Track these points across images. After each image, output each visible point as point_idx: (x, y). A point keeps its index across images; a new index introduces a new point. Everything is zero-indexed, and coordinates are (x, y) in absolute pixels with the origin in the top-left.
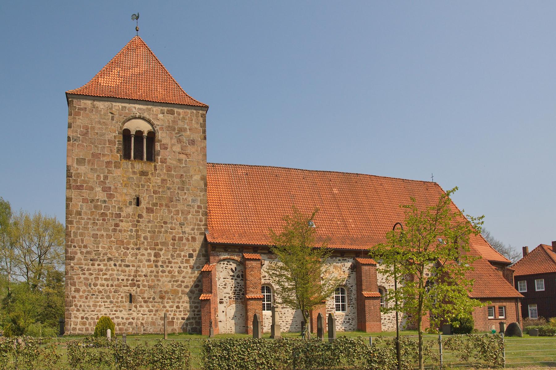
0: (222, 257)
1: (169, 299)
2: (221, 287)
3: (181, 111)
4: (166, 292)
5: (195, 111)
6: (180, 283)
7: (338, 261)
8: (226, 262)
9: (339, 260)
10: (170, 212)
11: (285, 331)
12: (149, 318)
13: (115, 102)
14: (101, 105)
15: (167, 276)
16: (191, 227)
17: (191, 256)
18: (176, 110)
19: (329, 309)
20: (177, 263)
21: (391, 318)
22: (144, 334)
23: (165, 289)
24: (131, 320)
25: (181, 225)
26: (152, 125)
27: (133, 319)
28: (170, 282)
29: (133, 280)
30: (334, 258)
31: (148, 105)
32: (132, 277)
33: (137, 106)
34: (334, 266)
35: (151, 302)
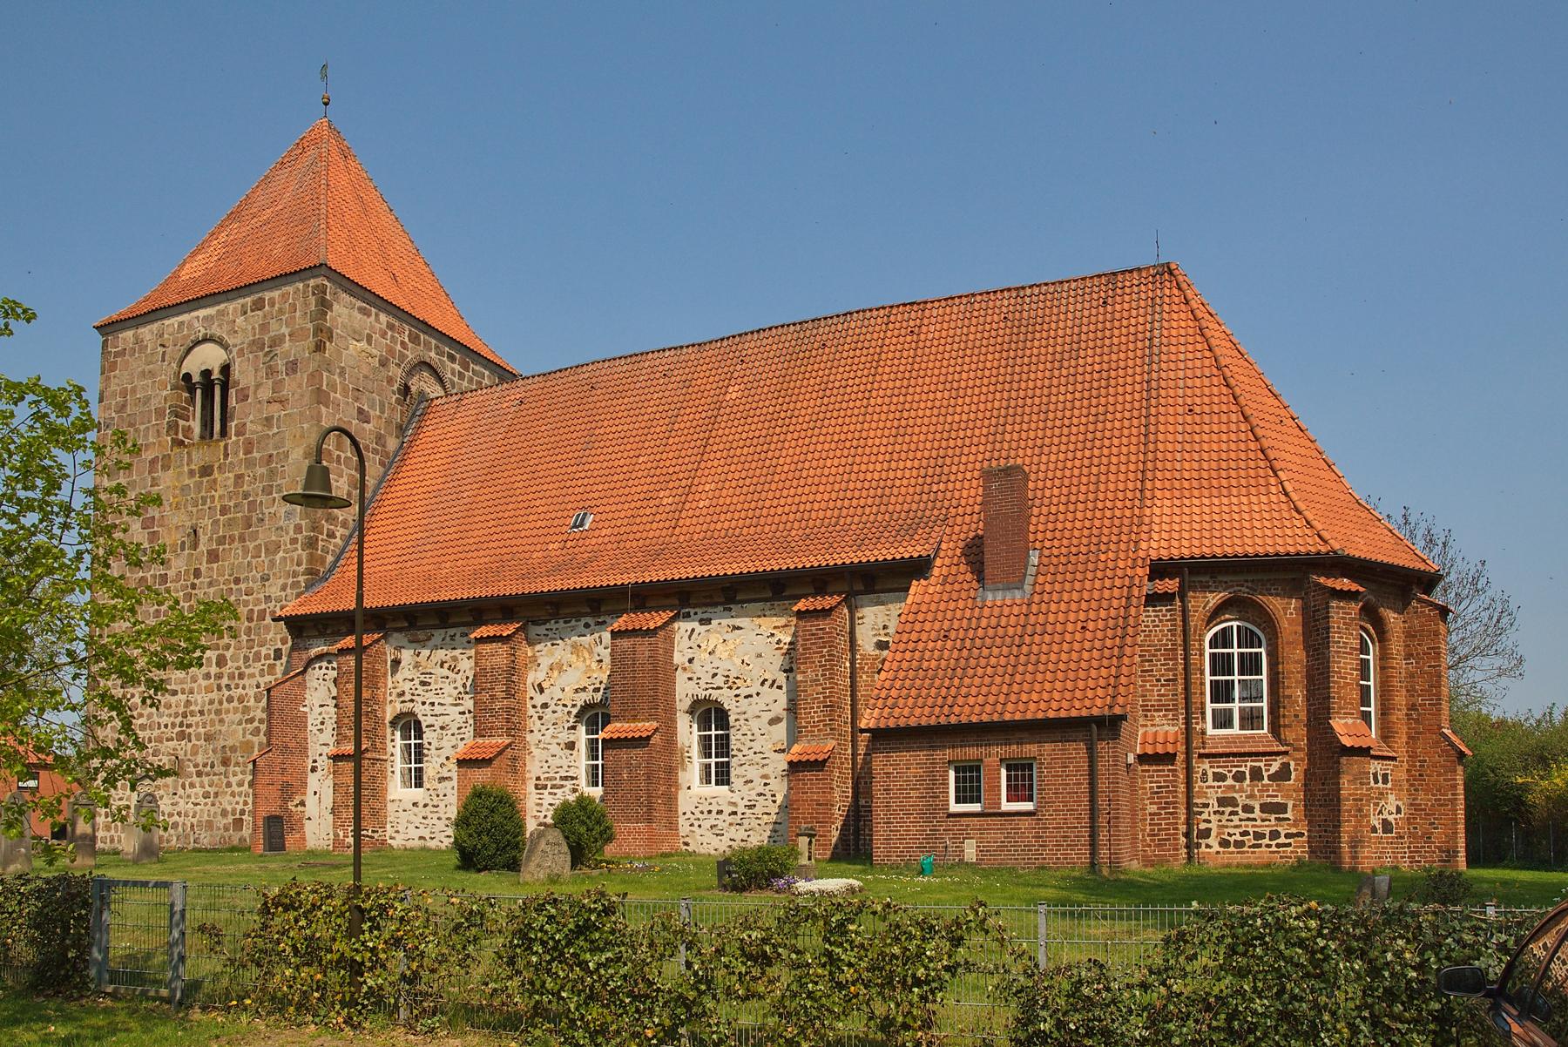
0: (313, 652)
1: (237, 764)
2: (315, 729)
3: (276, 294)
4: (233, 749)
5: (301, 286)
6: (256, 724)
7: (582, 629)
8: (324, 664)
9: (587, 626)
10: (246, 551)
11: (443, 847)
12: (205, 811)
13: (168, 317)
14: (147, 332)
15: (236, 710)
16: (281, 581)
17: (278, 654)
18: (267, 295)
19: (558, 782)
20: (252, 676)
21: (741, 809)
22: (195, 850)
23: (230, 743)
24: (176, 818)
25: (265, 579)
26: (225, 347)
27: (179, 814)
28: (240, 723)
29: (181, 725)
30: (573, 623)
31: (219, 303)
32: (180, 719)
33: (202, 313)
34: (574, 646)
35: (208, 774)
